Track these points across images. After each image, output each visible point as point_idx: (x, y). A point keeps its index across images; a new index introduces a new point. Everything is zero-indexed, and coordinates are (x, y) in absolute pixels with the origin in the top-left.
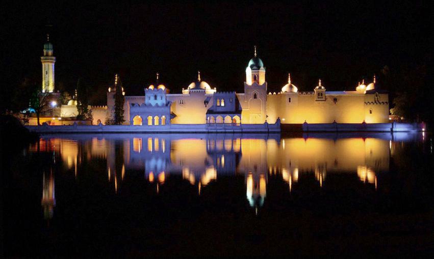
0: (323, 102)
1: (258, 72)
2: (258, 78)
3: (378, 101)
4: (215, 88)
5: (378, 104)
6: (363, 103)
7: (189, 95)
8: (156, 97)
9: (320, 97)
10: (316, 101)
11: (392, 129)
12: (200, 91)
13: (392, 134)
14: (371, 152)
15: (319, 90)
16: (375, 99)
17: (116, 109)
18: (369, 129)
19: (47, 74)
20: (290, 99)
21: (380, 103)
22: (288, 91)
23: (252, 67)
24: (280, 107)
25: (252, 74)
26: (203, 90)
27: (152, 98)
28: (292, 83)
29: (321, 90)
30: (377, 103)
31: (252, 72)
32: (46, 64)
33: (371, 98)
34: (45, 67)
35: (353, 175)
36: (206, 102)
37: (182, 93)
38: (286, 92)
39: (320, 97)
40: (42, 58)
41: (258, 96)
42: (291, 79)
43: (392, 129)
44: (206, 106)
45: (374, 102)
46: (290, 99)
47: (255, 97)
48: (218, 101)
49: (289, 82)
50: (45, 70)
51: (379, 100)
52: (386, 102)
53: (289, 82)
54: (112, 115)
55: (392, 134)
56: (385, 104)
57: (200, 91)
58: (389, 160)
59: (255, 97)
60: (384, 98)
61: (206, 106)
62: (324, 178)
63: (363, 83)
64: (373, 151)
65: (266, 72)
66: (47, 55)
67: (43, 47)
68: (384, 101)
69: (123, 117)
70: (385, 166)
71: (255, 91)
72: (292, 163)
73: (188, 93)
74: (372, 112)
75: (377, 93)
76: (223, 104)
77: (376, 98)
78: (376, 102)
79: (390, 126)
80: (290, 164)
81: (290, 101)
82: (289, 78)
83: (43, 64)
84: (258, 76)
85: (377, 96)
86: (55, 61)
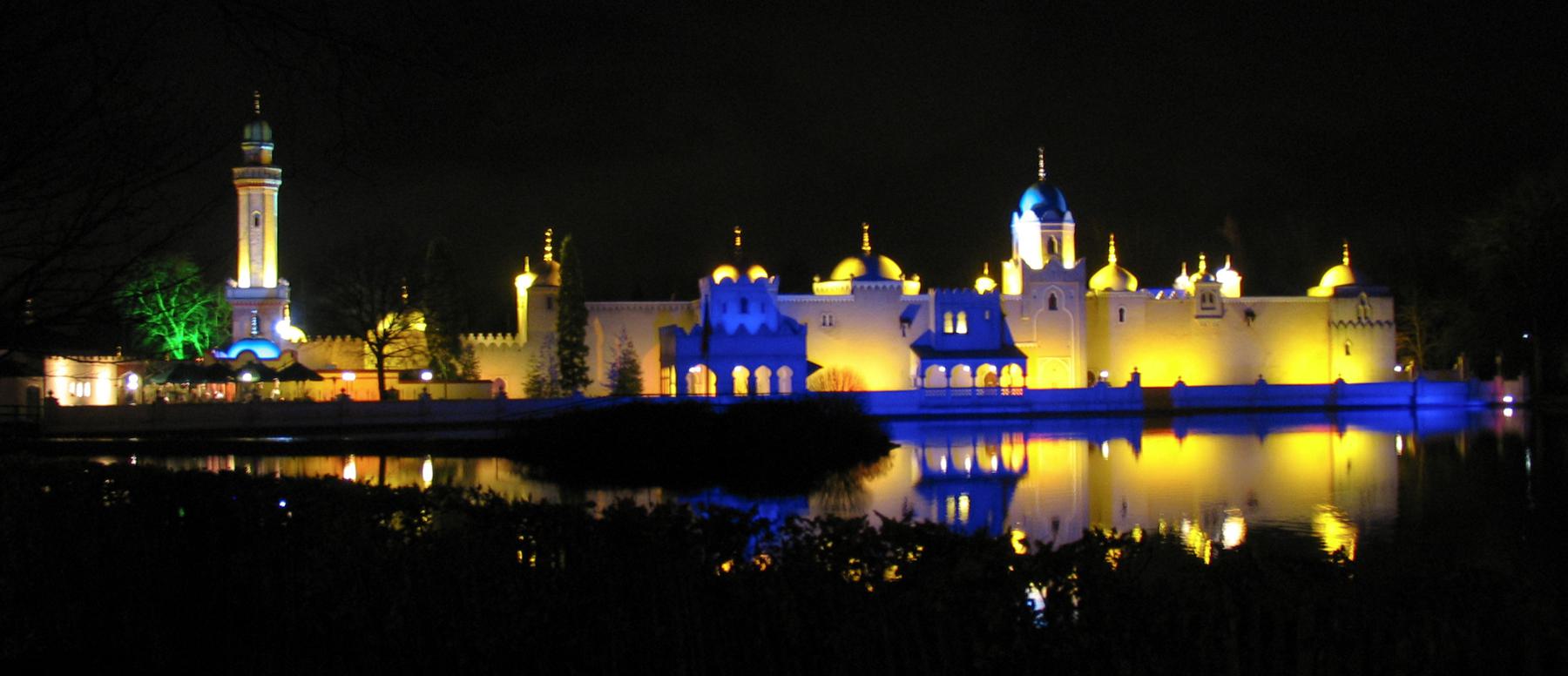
0: (1217, 320)
1: (1061, 228)
2: (1060, 248)
3: (1366, 318)
4: (917, 278)
5: (1368, 327)
6: (1323, 325)
7: (852, 298)
8: (744, 308)
9: (1208, 304)
10: (1198, 317)
11: (1413, 398)
12: (877, 288)
13: (1414, 415)
14: (1349, 466)
15: (1205, 285)
16: (1358, 311)
17: (563, 343)
18: (1357, 401)
19: (257, 224)
20: (1121, 311)
21: (1372, 325)
22: (1115, 288)
23: (1038, 210)
24: (1093, 342)
25: (1043, 235)
26: (895, 286)
27: (733, 308)
28: (1121, 263)
29: (1210, 285)
30: (1363, 325)
31: (1042, 228)
32: (255, 191)
33: (1348, 310)
34: (250, 203)
35: (1307, 541)
36: (906, 319)
37: (810, 291)
38: (1108, 290)
39: (1208, 304)
40: (237, 170)
41: (1060, 303)
42: (1116, 253)
43: (1413, 398)
44: (904, 335)
45: (1355, 321)
46: (1121, 311)
47: (1052, 304)
48: (948, 317)
49: (1112, 258)
50: (250, 212)
51: (1368, 315)
52: (1388, 322)
53: (1112, 258)
54: (543, 364)
55: (1414, 415)
56: (1386, 326)
57: (884, 287)
58: (1396, 486)
59: (1052, 304)
60: (1382, 309)
61: (904, 335)
62: (1299, 534)
63: (986, 271)
64: (1354, 464)
65: (1076, 227)
66: (257, 162)
67: (242, 133)
68: (1383, 319)
69: (587, 369)
70: (1386, 504)
71: (1056, 288)
72: (1353, 466)
73: (848, 293)
74: (1351, 350)
75: (1364, 295)
76: (962, 328)
77: (1361, 307)
78: (1363, 322)
79: (1409, 391)
80: (1124, 507)
81: (1121, 319)
82: (1112, 250)
83: (242, 193)
84: (1060, 241)
85: (1363, 303)
86: (279, 182)
